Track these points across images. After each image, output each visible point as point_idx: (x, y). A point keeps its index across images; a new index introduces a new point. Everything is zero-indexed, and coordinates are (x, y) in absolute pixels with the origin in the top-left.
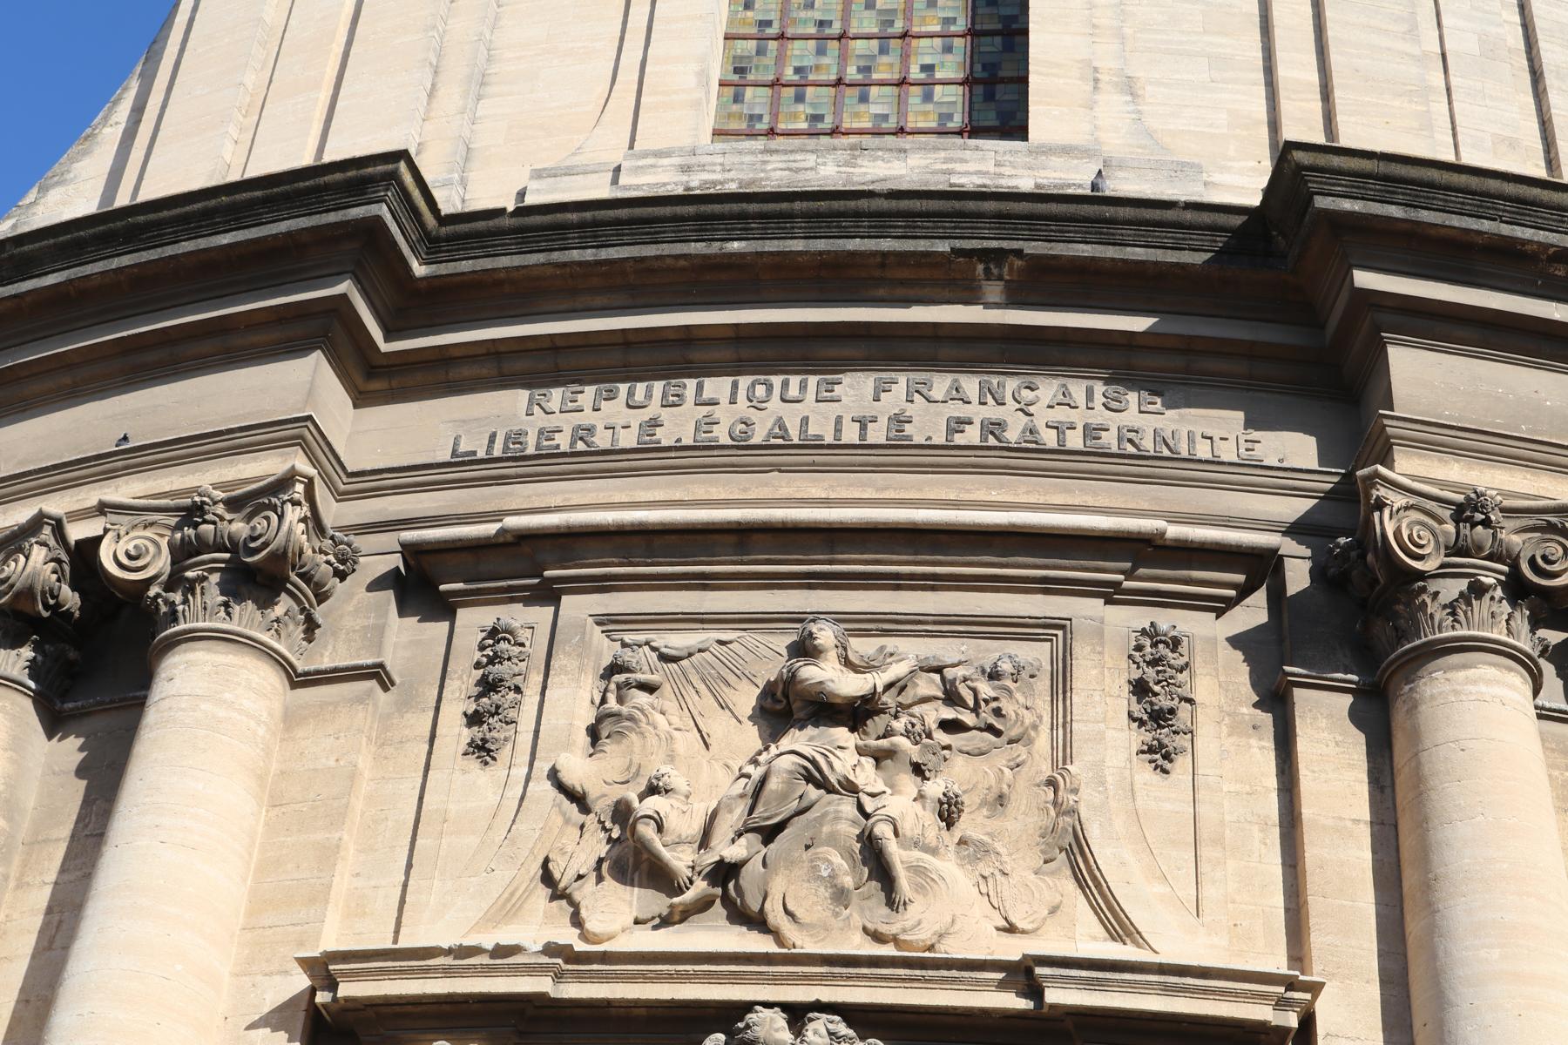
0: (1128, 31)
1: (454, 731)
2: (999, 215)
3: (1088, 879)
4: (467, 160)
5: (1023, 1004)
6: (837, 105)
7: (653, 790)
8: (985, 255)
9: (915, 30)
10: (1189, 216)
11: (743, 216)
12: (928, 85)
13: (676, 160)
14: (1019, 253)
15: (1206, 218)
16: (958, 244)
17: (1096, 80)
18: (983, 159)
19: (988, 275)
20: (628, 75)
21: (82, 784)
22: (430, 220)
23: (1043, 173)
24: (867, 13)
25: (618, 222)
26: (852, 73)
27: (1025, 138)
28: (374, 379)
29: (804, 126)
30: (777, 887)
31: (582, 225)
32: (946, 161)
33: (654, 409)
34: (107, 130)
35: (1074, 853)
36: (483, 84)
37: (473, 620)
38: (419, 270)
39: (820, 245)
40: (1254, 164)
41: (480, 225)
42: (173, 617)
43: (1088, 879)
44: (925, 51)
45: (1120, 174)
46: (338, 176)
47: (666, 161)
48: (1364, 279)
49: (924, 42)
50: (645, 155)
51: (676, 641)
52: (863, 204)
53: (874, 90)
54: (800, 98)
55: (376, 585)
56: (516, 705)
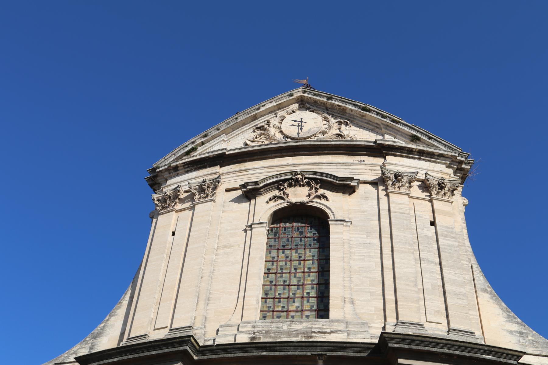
0: (352, 286)
2: (321, 346)
4: (205, 321)
6: (288, 303)
8: (319, 355)
9: (305, 283)
10: (362, 345)
11: (265, 347)
12: (308, 298)
13: (252, 324)
14: (326, 354)
15: (366, 346)
16: (312, 353)
17: (345, 301)
18: (319, 324)
19: (319, 359)
20: (241, 300)
22: (198, 347)
23: (332, 327)
24: (295, 279)
25: (238, 348)
26: (291, 295)
27: (328, 318)
29: (280, 309)
31: (230, 348)
32: (311, 324)
34: (124, 302)
36: (209, 300)
38: (195, 358)
39: (282, 353)
40: (380, 321)
41: (209, 348)
44: (308, 289)
45: (350, 326)
46: (178, 340)
47: (249, 325)
48: (400, 361)
49: (307, 286)
50: (245, 323)
52: (292, 344)
53: (296, 299)
54: (279, 302)
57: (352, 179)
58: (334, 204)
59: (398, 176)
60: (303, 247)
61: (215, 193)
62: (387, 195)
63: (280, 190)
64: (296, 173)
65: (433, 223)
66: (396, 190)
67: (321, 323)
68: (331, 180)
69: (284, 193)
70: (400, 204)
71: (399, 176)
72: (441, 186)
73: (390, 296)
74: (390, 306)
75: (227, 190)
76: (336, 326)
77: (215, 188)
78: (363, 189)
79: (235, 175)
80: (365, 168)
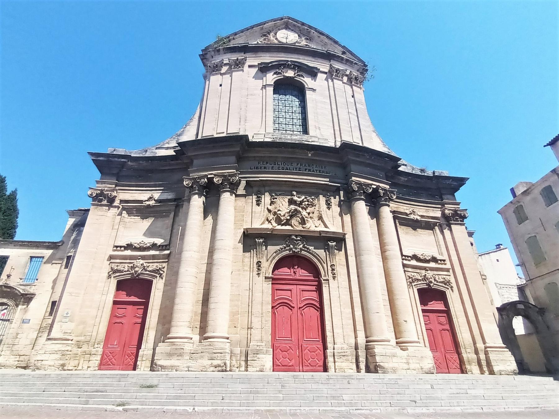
3: (323, 222)
5: (292, 229)
7: (279, 210)
20: (264, 122)
30: (293, 222)
35: (320, 218)
43: (323, 222)
58: (307, 81)
64: (288, 61)
65: (353, 96)
67: (305, 137)
73: (337, 128)
74: (337, 133)
76: (313, 139)
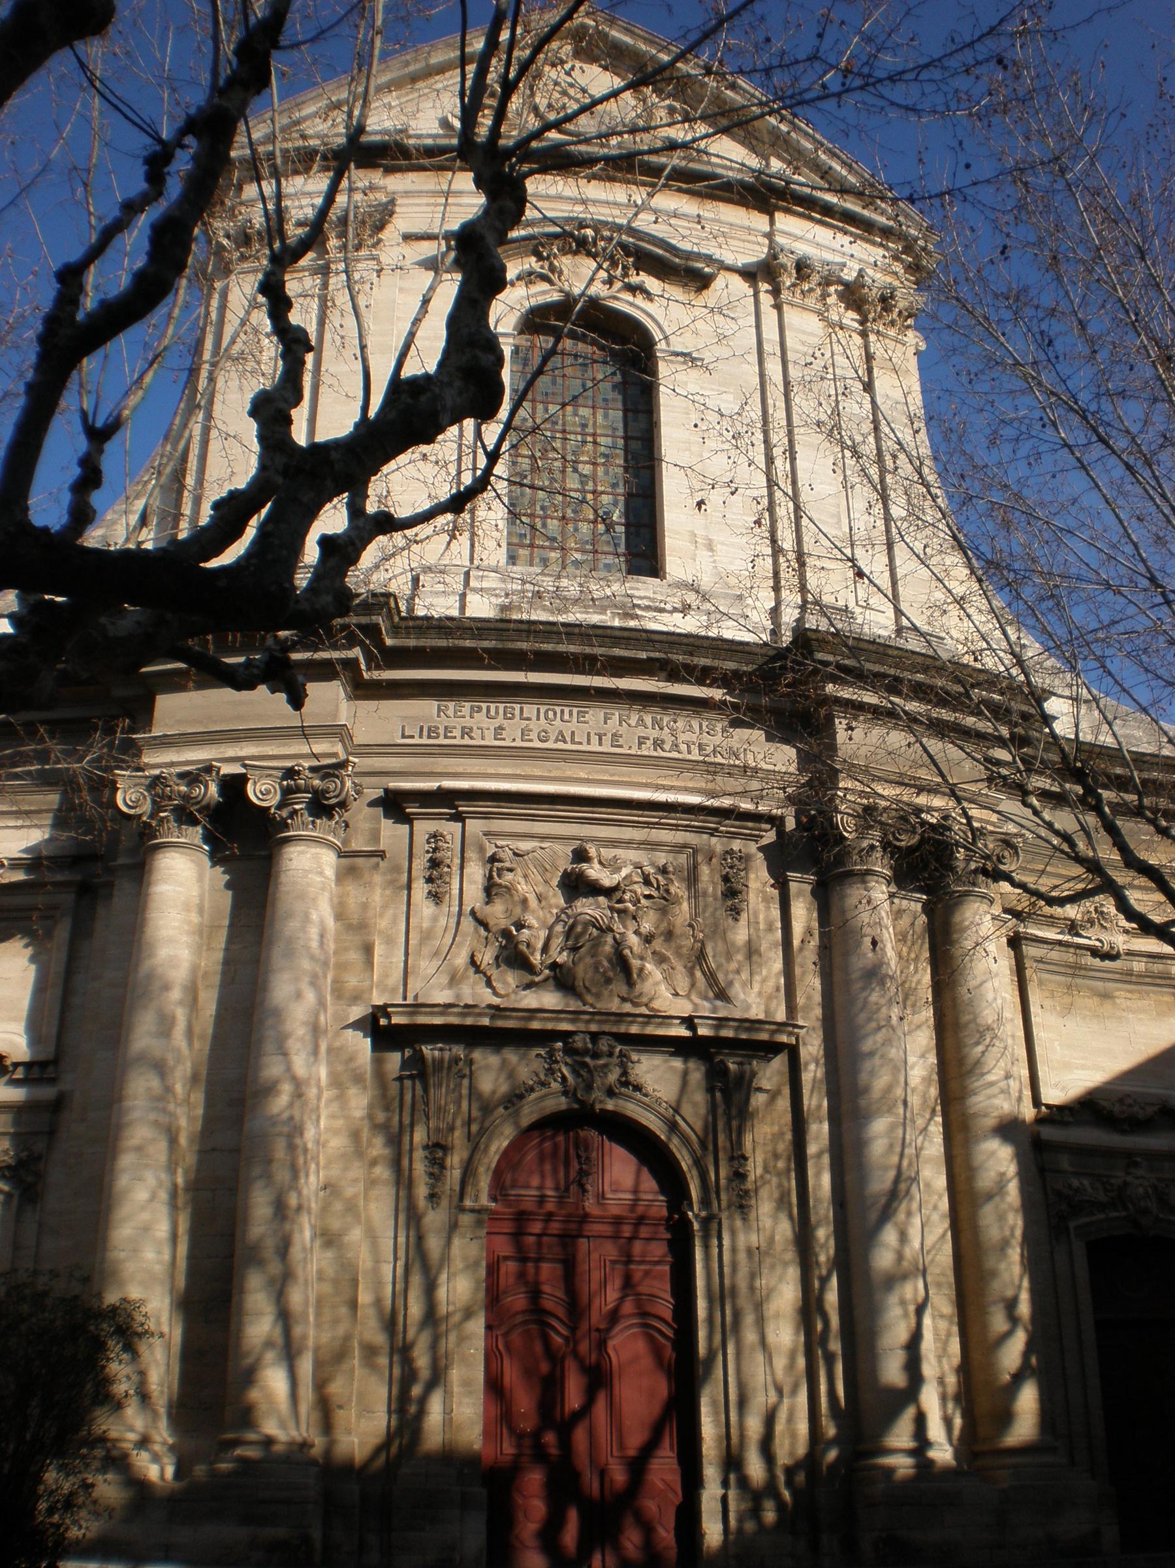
1: (420, 889)
21: (230, 893)
22: (396, 619)
27: (663, 578)
28: (363, 690)
33: (500, 720)
37: (423, 828)
38: (389, 642)
42: (285, 826)
51: (524, 846)
55: (373, 804)
56: (450, 874)
57: (709, 259)
59: (802, 268)
60: (590, 403)
61: (380, 241)
62: (778, 307)
63: (540, 257)
64: (582, 225)
66: (797, 300)
67: (644, 588)
68: (660, 252)
69: (552, 269)
70: (804, 332)
71: (808, 267)
72: (886, 301)
75: (408, 237)
77: (380, 227)
78: (730, 287)
79: (424, 200)
80: (733, 235)
